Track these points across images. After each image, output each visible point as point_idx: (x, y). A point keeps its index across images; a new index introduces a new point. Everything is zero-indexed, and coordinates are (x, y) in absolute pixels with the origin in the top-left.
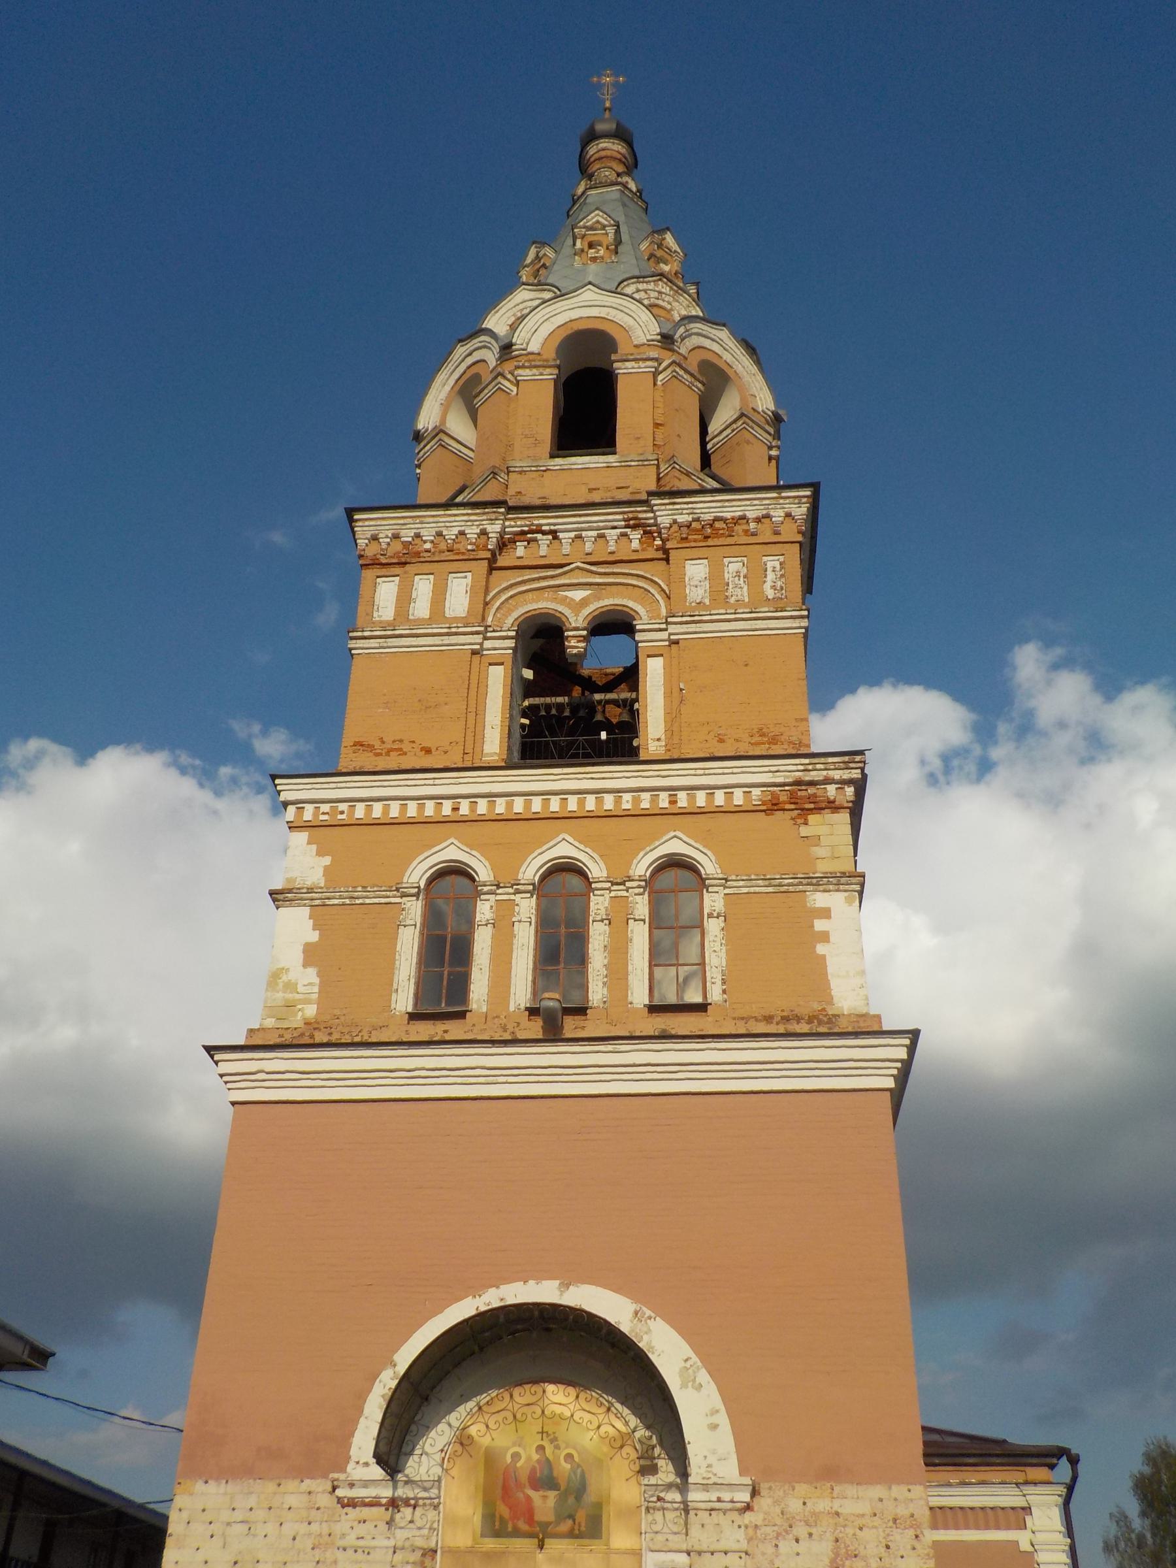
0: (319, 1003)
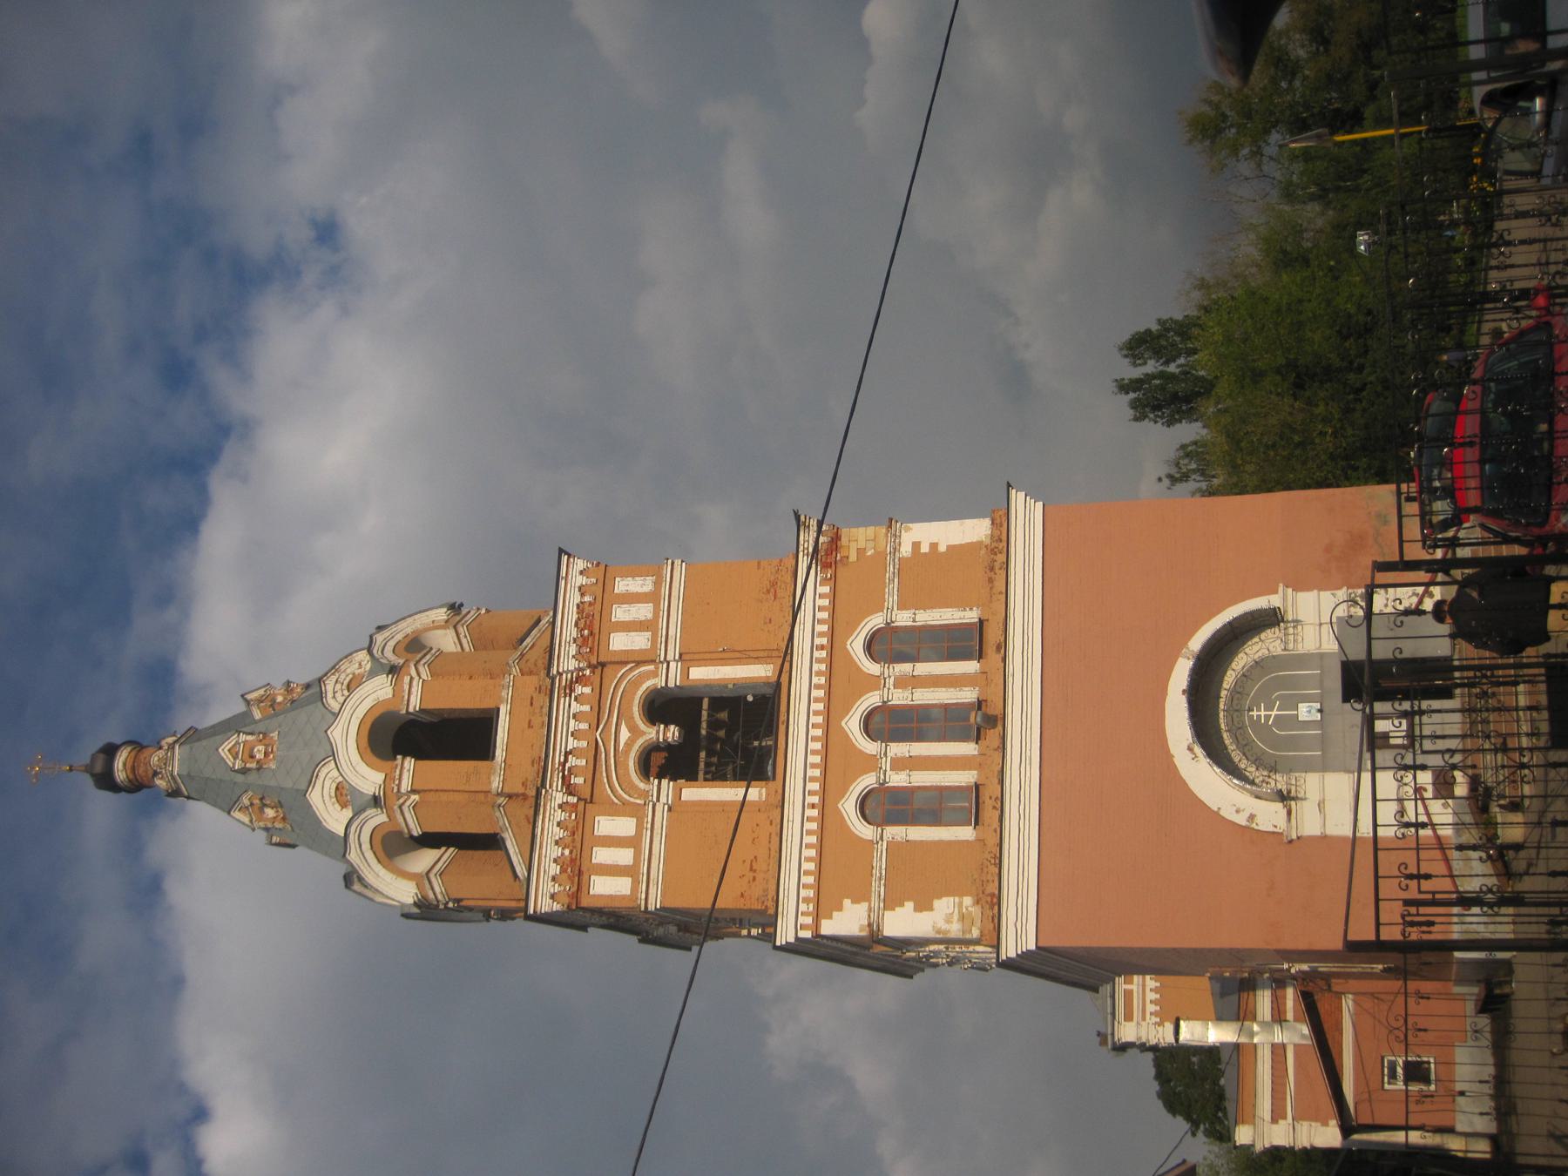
0: (961, 895)
